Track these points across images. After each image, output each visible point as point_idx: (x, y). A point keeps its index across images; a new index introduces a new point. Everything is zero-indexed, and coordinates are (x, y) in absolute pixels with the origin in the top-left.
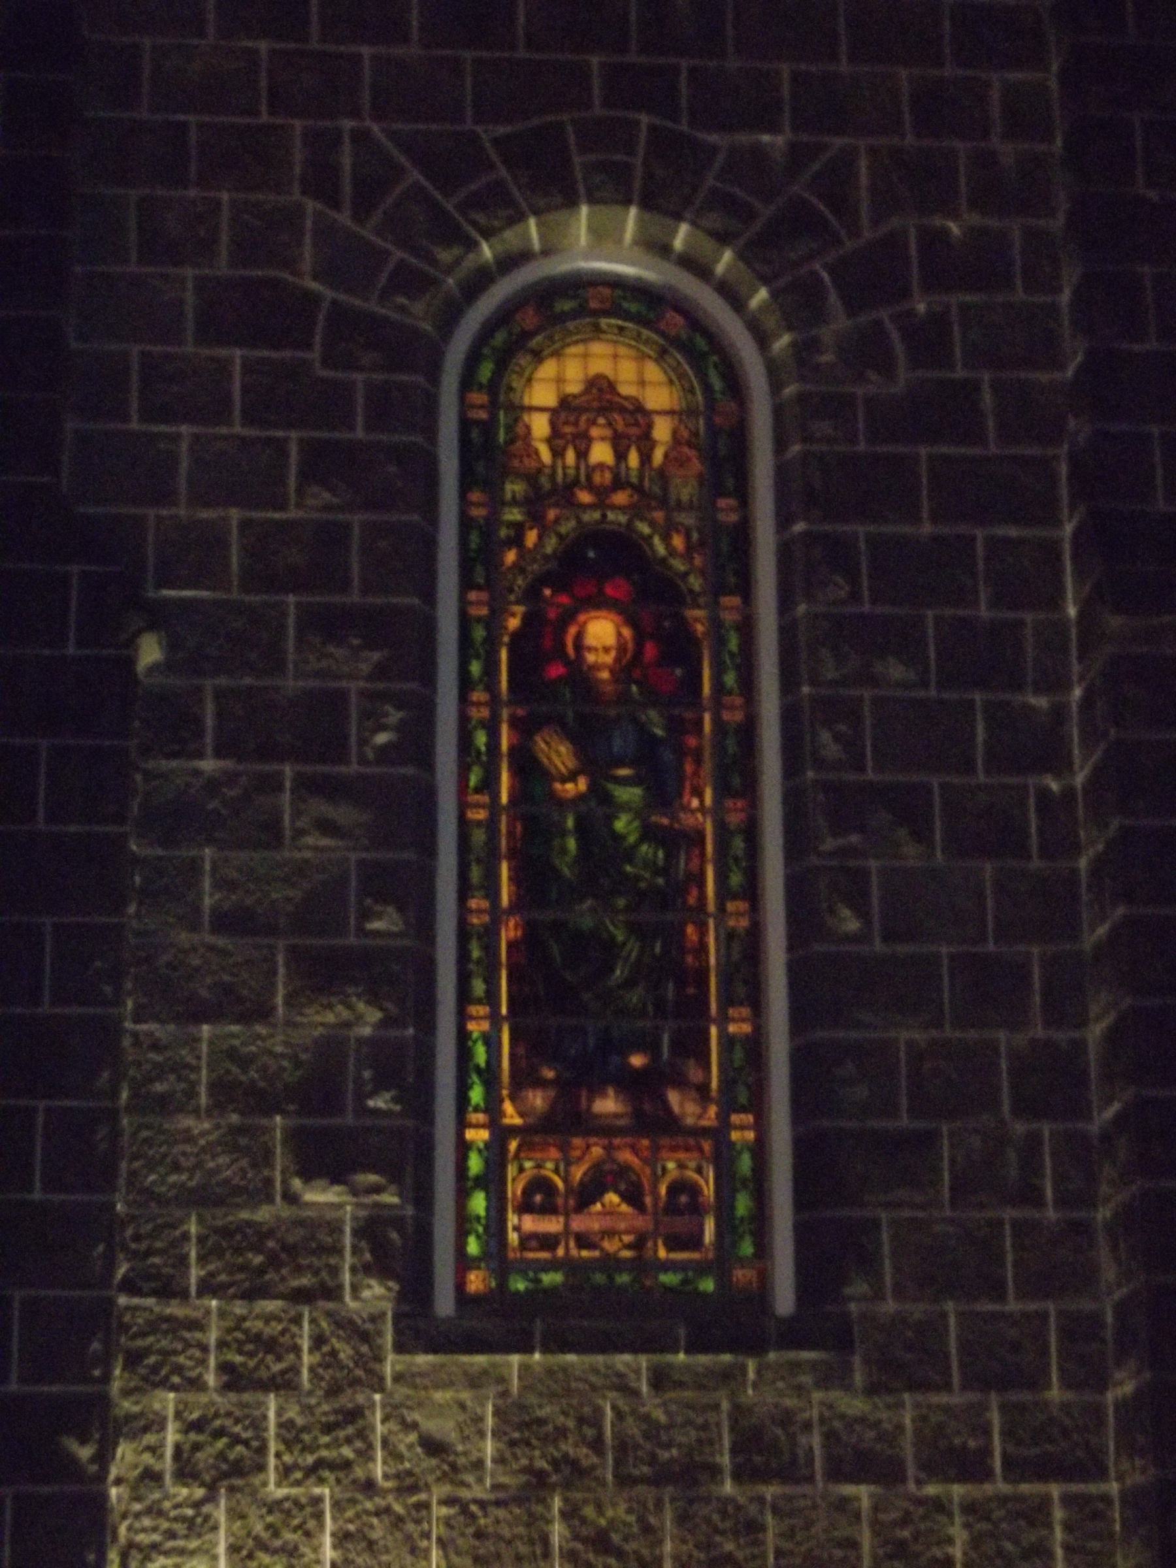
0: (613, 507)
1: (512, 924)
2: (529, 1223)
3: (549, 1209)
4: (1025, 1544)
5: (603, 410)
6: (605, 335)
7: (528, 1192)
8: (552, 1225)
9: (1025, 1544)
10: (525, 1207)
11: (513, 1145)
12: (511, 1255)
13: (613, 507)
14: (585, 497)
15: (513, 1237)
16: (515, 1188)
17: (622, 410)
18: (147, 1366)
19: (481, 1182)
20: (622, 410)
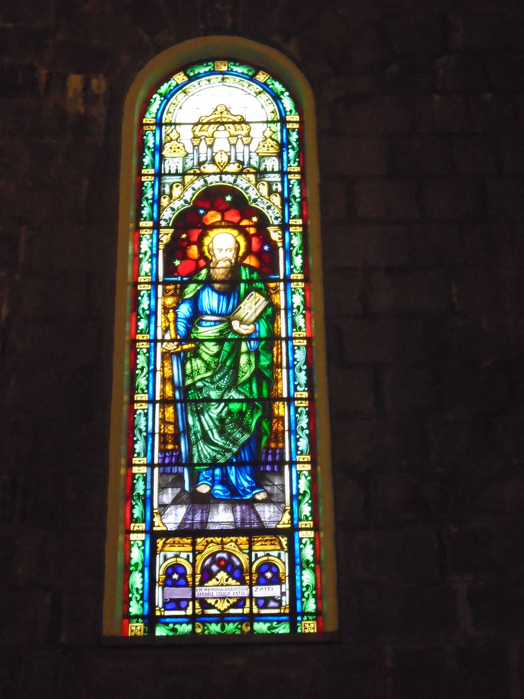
6: (220, 121)
9: (227, 577)
10: (169, 582)
11: (160, 543)
14: (209, 168)
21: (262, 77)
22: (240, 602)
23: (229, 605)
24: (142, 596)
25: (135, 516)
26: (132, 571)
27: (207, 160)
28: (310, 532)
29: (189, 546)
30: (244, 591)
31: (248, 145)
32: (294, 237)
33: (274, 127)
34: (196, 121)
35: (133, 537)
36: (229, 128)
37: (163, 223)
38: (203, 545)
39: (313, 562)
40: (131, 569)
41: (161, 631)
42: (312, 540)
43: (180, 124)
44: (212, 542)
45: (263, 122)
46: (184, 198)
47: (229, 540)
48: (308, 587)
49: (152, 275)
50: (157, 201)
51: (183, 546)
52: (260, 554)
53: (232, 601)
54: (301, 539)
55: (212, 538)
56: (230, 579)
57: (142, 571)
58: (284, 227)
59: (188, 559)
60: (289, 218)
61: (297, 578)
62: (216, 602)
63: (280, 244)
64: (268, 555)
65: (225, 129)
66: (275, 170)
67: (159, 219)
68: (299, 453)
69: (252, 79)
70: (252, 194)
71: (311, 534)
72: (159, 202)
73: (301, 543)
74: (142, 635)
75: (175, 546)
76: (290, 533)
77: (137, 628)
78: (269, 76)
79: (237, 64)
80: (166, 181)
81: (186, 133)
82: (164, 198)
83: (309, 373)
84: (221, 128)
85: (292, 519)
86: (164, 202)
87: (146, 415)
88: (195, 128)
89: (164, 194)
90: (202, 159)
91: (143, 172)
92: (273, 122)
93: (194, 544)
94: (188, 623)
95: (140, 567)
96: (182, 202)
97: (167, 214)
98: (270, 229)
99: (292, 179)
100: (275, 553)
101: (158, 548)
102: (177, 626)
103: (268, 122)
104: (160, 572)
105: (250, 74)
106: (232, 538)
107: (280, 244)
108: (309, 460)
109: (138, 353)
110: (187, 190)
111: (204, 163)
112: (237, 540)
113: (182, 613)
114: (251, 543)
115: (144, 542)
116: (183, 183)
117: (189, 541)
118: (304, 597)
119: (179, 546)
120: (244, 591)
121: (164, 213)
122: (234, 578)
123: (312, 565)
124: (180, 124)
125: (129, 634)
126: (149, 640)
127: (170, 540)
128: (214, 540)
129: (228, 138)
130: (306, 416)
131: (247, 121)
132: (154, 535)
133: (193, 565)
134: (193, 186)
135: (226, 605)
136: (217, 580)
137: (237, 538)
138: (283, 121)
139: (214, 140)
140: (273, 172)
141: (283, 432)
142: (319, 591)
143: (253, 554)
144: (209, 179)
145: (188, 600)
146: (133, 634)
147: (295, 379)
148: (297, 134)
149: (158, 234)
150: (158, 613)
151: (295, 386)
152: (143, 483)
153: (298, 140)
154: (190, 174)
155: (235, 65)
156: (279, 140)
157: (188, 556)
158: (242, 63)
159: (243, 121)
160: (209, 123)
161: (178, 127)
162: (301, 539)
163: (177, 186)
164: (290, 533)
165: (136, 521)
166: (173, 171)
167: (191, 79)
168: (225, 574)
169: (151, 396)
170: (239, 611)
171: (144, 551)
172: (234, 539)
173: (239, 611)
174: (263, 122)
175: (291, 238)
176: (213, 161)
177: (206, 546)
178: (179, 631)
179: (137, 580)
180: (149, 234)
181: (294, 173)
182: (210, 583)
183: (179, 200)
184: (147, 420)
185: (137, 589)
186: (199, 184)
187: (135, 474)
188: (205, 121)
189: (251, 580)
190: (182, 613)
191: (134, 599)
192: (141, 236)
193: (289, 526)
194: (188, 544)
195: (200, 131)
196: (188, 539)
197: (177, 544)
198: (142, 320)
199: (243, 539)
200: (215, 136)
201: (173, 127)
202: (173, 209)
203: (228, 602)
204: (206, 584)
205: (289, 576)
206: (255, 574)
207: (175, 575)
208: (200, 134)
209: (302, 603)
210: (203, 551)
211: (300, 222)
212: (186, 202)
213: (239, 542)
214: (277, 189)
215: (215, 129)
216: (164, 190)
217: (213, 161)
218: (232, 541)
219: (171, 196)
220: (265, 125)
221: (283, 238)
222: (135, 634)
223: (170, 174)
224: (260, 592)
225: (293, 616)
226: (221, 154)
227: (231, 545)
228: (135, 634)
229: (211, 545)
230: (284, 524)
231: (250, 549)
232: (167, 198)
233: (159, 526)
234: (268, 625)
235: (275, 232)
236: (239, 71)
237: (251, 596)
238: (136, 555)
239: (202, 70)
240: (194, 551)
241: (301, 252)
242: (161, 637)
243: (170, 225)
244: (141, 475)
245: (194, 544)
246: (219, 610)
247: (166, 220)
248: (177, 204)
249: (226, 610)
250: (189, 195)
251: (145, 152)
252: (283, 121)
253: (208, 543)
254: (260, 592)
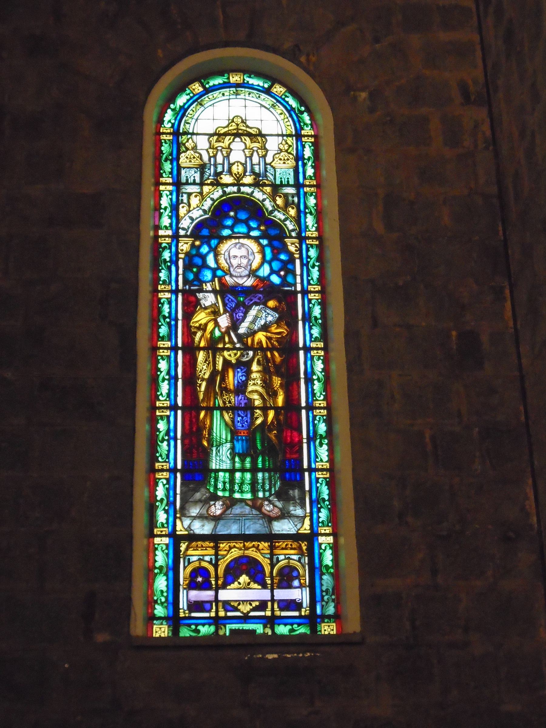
0: (244, 185)
1: (292, 508)
2: (196, 595)
3: (206, 586)
4: (249, 581)
5: (237, 135)
6: (238, 125)
7: (194, 573)
8: (207, 595)
9: (249, 581)
10: (193, 585)
11: (183, 547)
12: (182, 615)
13: (244, 185)
14: (226, 179)
15: (183, 604)
16: (184, 574)
17: (249, 135)
18: (203, 400)
19: (305, 265)
20: (249, 135)
21: (278, 89)
22: (263, 605)
23: (251, 607)
24: (167, 598)
25: (161, 335)
26: (156, 574)
27: (223, 171)
28: (329, 537)
29: (211, 549)
30: (265, 595)
31: (264, 157)
32: (310, 249)
33: (290, 140)
34: (212, 132)
35: (157, 540)
36: (245, 140)
37: (182, 233)
38: (226, 550)
39: (320, 319)
40: (156, 571)
41: (185, 632)
42: (331, 545)
43: (197, 134)
44: (235, 547)
45: (278, 135)
46: (203, 208)
47: (251, 545)
48: (327, 591)
49: (170, 400)
50: (175, 208)
51: (206, 550)
52: (281, 557)
53: (254, 604)
54: (320, 545)
55: (234, 544)
56: (252, 583)
57: (166, 574)
58: (301, 239)
59: (210, 562)
60: (311, 341)
61: (302, 220)
62: (239, 604)
63: (297, 256)
64: (289, 558)
65: (242, 141)
66: (290, 183)
67: (178, 228)
68: (320, 525)
69: (268, 91)
70: (268, 205)
71: (330, 539)
72: (177, 210)
73: (320, 548)
74: (166, 635)
75: (198, 550)
76: (311, 538)
77: (161, 631)
78: (285, 90)
79: (252, 76)
80: (184, 190)
81: (202, 143)
82: (183, 207)
83: (321, 248)
84: (237, 139)
85: (311, 525)
86: (182, 211)
87: (170, 303)
88: (211, 139)
89: (182, 202)
90: (220, 169)
91: (160, 234)
92: (288, 136)
93: (216, 548)
94: (210, 625)
95: (165, 570)
96: (201, 212)
97: (185, 223)
98: (288, 241)
99: (317, 415)
100: (296, 557)
101: (181, 551)
102: (200, 627)
103: (283, 135)
104: (184, 574)
105: (266, 86)
106: (254, 543)
107: (297, 256)
108: (331, 532)
109: (156, 549)
110: (206, 201)
111: (221, 173)
112: (259, 545)
113: (206, 615)
114: (272, 548)
115: (167, 545)
116: (201, 193)
117: (212, 544)
118: (324, 601)
119: (202, 550)
120: (265, 595)
121: (183, 221)
122: (255, 582)
123: (320, 321)
124: (197, 134)
125: (154, 635)
126: (174, 643)
127: (194, 544)
128: (237, 546)
129: (243, 151)
130: (326, 487)
131: (263, 132)
132: (176, 539)
133: (216, 566)
134: (212, 196)
135: (248, 608)
136: (239, 583)
137: (259, 543)
138: (298, 136)
139: (231, 152)
140: (288, 185)
141: (301, 442)
142: (319, 207)
143: (275, 557)
144: (229, 190)
145: (210, 602)
146: (158, 635)
147: (308, 275)
148: (323, 363)
149: (178, 242)
150: (182, 615)
151: (308, 281)
152: (168, 306)
153: (324, 370)
154: (208, 184)
155: (250, 77)
156: (294, 153)
157: (211, 559)
158: (259, 75)
159: (261, 134)
160: (226, 134)
161: (194, 137)
162: (320, 545)
163: (196, 196)
164: (311, 538)
165: (163, 339)
166: (191, 180)
167: (207, 91)
168: (247, 578)
169: (173, 403)
170: (262, 613)
171: (167, 555)
172: (256, 543)
173: (262, 613)
174: (278, 135)
175: (308, 250)
176: (230, 172)
177: (229, 551)
178: (201, 631)
179: (161, 583)
180: (165, 479)
181: (322, 470)
182: (232, 586)
183: (198, 210)
184: (170, 308)
185: (162, 592)
186: (217, 193)
187: (161, 298)
188: (222, 132)
189: (272, 584)
190: (206, 615)
191: (159, 549)
192: (157, 480)
193: (309, 532)
194: (209, 547)
195: (216, 142)
196: (210, 543)
197: (200, 547)
198: (162, 327)
199: (264, 545)
200: (231, 147)
201: (189, 136)
202: (192, 219)
203: (251, 604)
204: (228, 587)
205: (308, 564)
206: (276, 577)
207: (200, 579)
208: (217, 145)
209: (322, 606)
210: (226, 555)
211: (321, 345)
212: (204, 211)
213: (261, 547)
214: (293, 201)
215: (231, 140)
216: (182, 200)
217: (230, 172)
218: (254, 546)
219: (189, 206)
220: (281, 138)
221: (300, 250)
222: (160, 636)
223: (187, 183)
224: (281, 594)
225: (313, 620)
226: (238, 166)
227: (253, 551)
228: (160, 636)
229: (233, 550)
230: (305, 529)
231: (272, 554)
232: (186, 208)
233: (181, 530)
234: (289, 627)
235: (292, 244)
236: (254, 84)
237: (273, 600)
238: (161, 559)
239: (218, 81)
240: (216, 555)
241: (317, 264)
242: (185, 638)
243: (189, 233)
244: (165, 300)
245: (216, 548)
246: (242, 612)
247: (183, 229)
248: (197, 214)
249: (248, 612)
250: (207, 204)
251: (160, 322)
252: (298, 136)
253: (231, 548)
254: (281, 594)
